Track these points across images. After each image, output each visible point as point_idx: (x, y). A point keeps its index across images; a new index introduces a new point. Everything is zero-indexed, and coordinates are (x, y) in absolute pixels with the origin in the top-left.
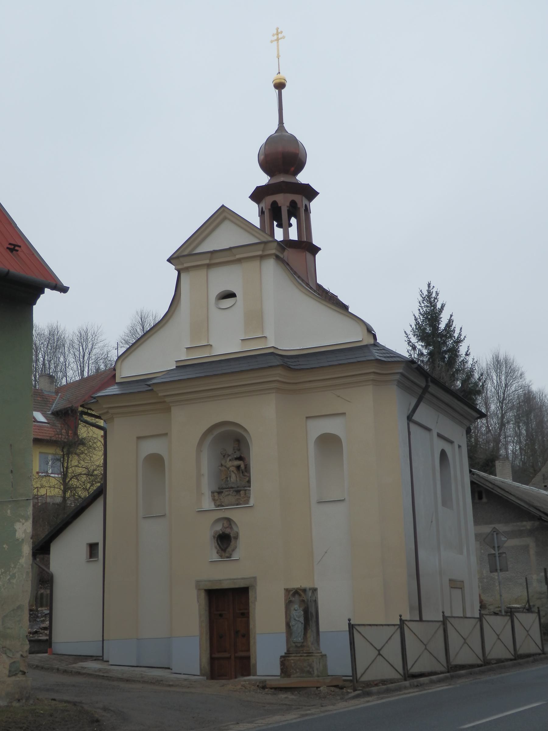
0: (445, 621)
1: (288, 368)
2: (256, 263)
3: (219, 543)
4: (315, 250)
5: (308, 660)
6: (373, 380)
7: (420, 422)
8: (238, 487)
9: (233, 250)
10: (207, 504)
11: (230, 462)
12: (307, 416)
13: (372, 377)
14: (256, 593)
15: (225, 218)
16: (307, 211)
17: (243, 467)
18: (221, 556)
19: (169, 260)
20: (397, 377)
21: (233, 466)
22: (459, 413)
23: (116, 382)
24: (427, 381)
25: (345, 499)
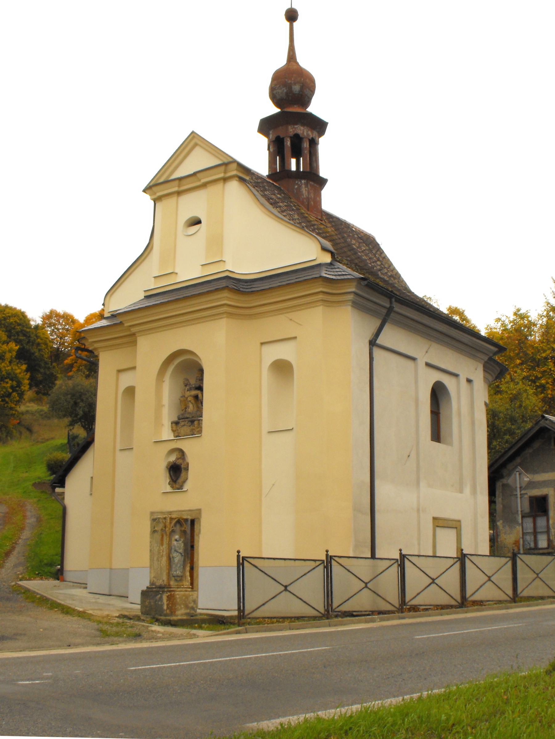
1: (237, 291)
2: (220, 185)
3: (172, 474)
4: (322, 182)
5: (192, 595)
6: (322, 300)
7: (392, 348)
8: (193, 417)
9: (198, 175)
10: (167, 434)
11: (188, 392)
13: (321, 296)
14: (200, 526)
15: (196, 145)
18: (172, 487)
19: (144, 191)
20: (351, 297)
21: (191, 396)
22: (464, 344)
23: (105, 316)
24: (391, 303)
25: (293, 429)
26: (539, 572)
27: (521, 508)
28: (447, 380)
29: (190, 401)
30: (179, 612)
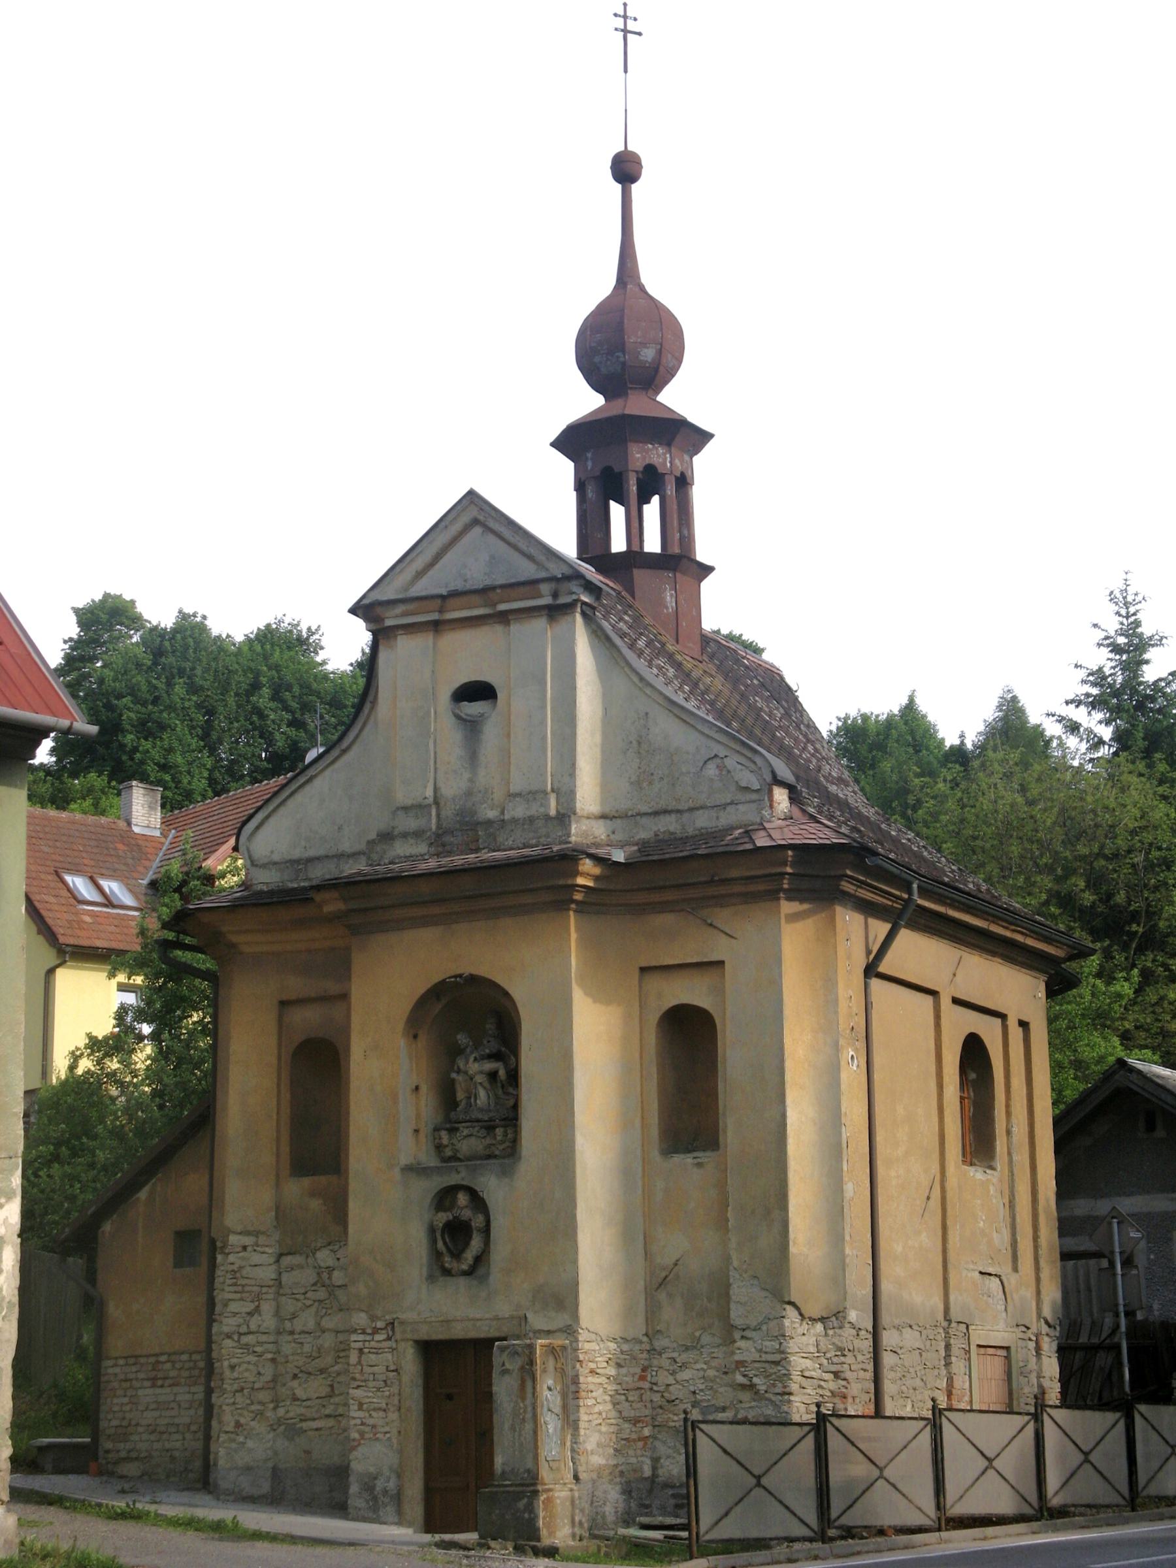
0: (935, 1421)
3: (447, 1240)
12: (644, 964)
16: (684, 482)
17: (502, 1073)
21: (481, 1072)
26: (764, 1469)
27: (1124, 1299)
28: (990, 1032)
29: (480, 1083)
30: (559, 1534)
